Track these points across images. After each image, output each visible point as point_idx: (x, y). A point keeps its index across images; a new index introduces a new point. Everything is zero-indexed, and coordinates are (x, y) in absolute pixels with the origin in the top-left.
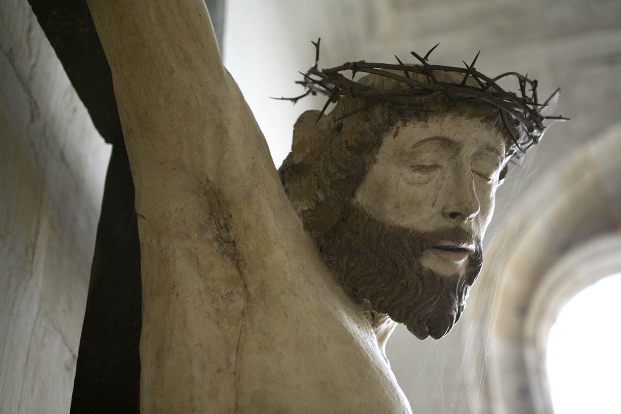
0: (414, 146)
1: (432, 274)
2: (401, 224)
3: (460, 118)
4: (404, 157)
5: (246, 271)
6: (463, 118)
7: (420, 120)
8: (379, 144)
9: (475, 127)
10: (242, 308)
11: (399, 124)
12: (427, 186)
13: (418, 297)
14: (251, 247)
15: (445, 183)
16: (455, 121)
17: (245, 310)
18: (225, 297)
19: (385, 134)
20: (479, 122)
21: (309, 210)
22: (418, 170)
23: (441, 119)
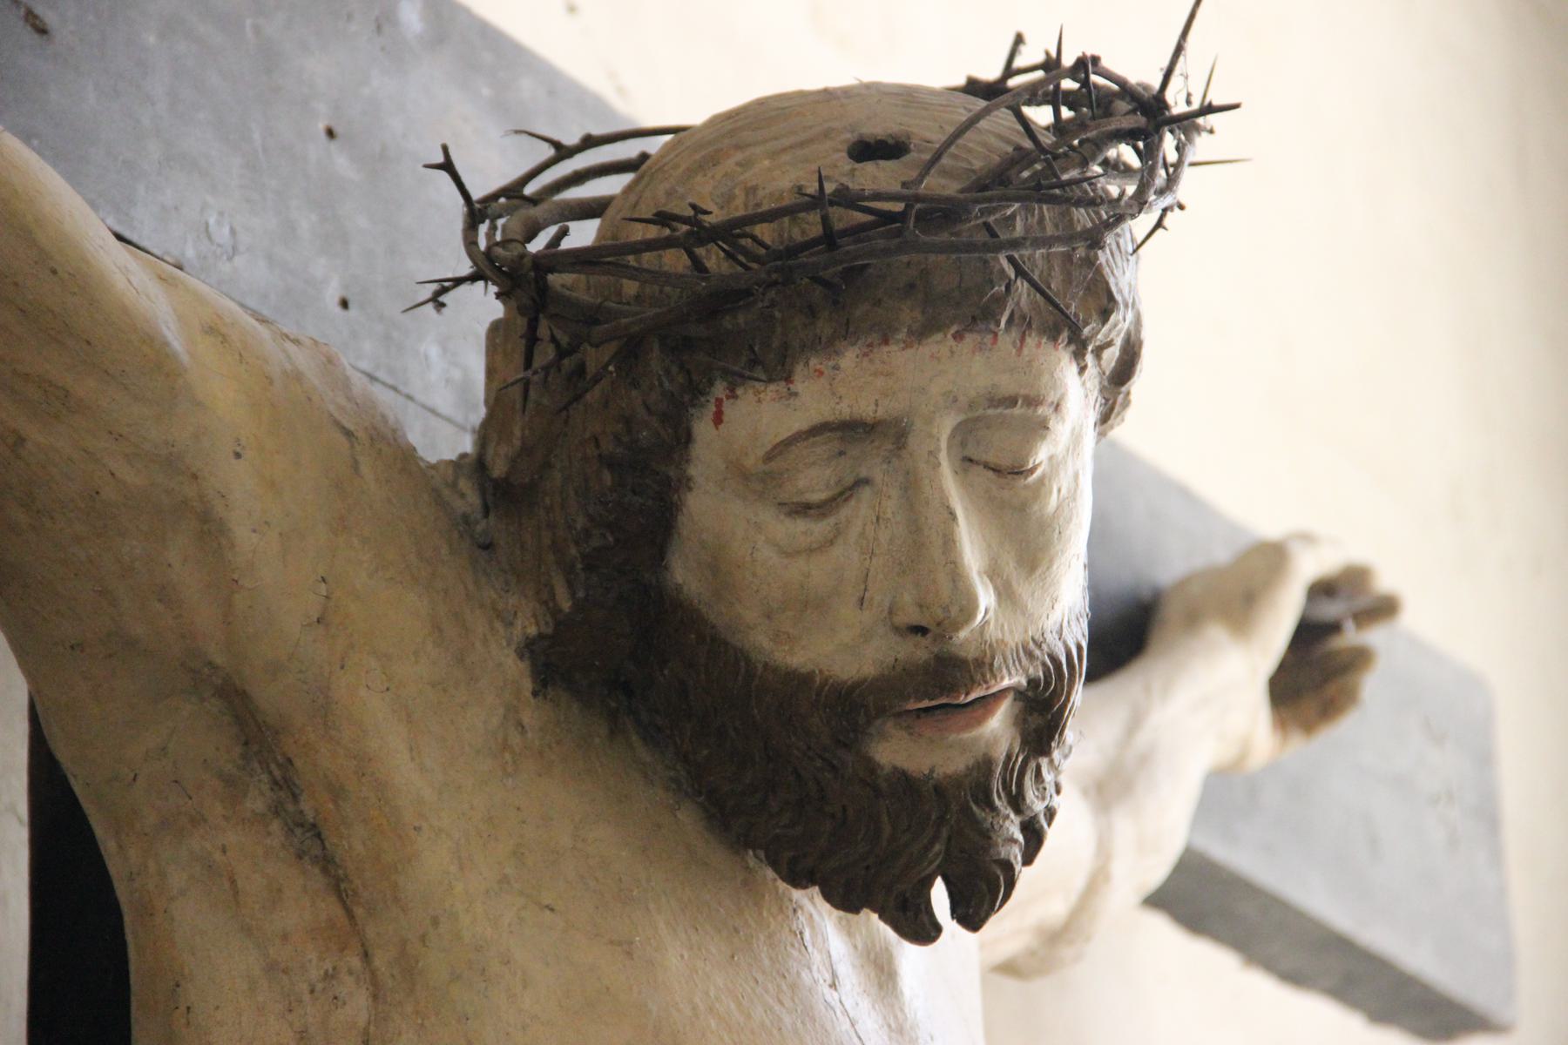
0: (769, 457)
1: (906, 784)
2: (789, 660)
3: (885, 349)
4: (761, 479)
5: (359, 911)
6: (893, 348)
7: (770, 380)
8: (686, 439)
9: (939, 359)
10: (362, 1021)
11: (720, 389)
12: (837, 551)
13: (884, 843)
14: (359, 848)
15: (884, 536)
16: (871, 361)
17: (372, 1028)
18: (319, 986)
19: (692, 411)
20: (951, 342)
21: (541, 636)
22: (797, 512)
23: (831, 363)
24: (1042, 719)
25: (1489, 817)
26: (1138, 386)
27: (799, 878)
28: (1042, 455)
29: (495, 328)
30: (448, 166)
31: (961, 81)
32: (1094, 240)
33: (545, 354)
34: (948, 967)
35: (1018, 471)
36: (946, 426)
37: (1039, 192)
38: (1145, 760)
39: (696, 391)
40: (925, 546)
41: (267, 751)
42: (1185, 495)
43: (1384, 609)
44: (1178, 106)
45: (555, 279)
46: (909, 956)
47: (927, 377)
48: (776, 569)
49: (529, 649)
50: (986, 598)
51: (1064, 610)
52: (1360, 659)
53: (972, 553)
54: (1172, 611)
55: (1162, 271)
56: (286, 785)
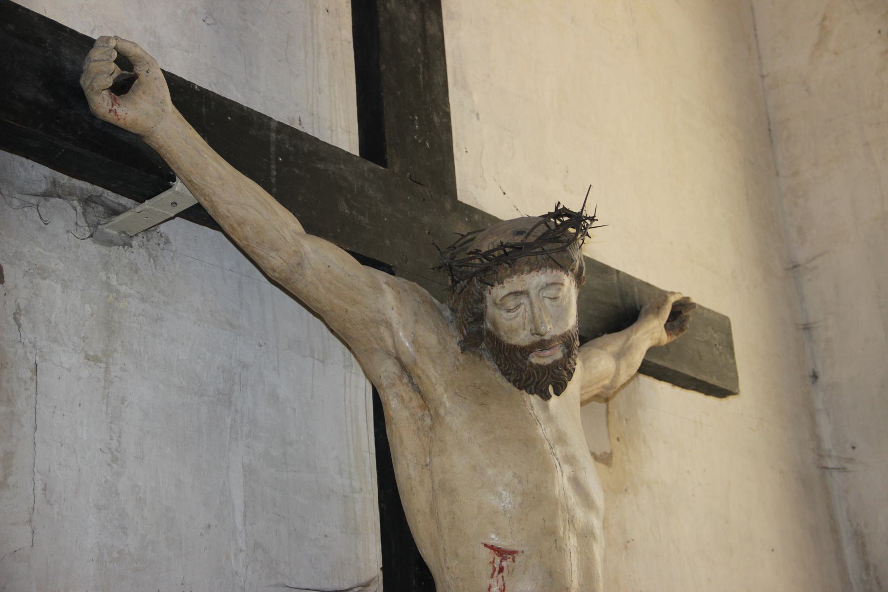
37: (556, 240)
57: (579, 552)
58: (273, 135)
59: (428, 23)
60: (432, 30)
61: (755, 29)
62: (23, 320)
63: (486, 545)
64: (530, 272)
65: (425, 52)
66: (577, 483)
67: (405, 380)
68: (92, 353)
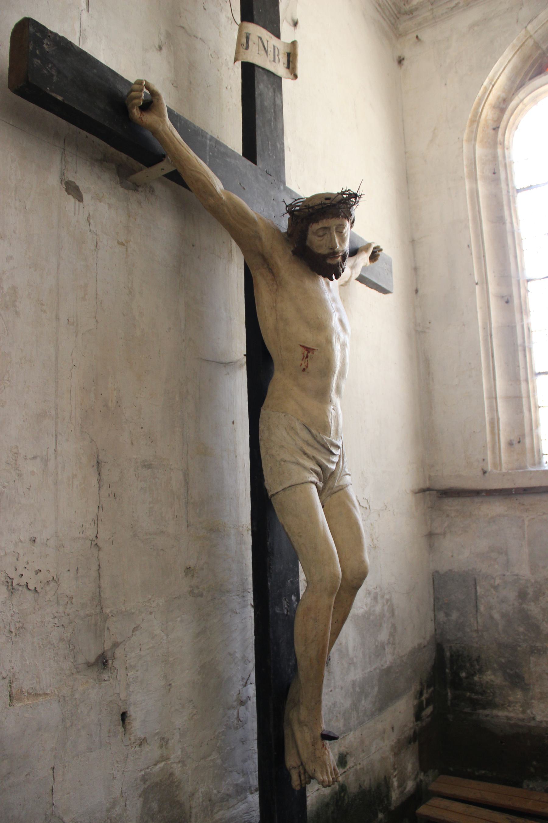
4: (315, 233)
8: (308, 229)
24: (344, 258)
25: (391, 272)
26: (355, 224)
27: (320, 274)
28: (344, 231)
29: (289, 219)
30: (284, 201)
31: (287, 70)
32: (350, 208)
33: (294, 220)
34: (335, 283)
35: (342, 232)
36: (334, 228)
38: (356, 265)
39: (309, 224)
40: (332, 240)
41: (266, 262)
42: (361, 238)
43: (381, 250)
44: (358, 194)
45: (295, 213)
46: (331, 283)
47: (333, 223)
48: (317, 243)
49: (292, 251)
50: (338, 246)
51: (347, 247)
52: (378, 255)
53: (337, 241)
54: (360, 250)
55: (357, 211)
56: (268, 265)
57: (341, 352)
58: (208, 142)
59: (276, 98)
60: (278, 102)
61: (404, 130)
62: (91, 221)
63: (301, 346)
64: (332, 218)
65: (275, 112)
66: (341, 322)
67: (265, 266)
68: (120, 241)
